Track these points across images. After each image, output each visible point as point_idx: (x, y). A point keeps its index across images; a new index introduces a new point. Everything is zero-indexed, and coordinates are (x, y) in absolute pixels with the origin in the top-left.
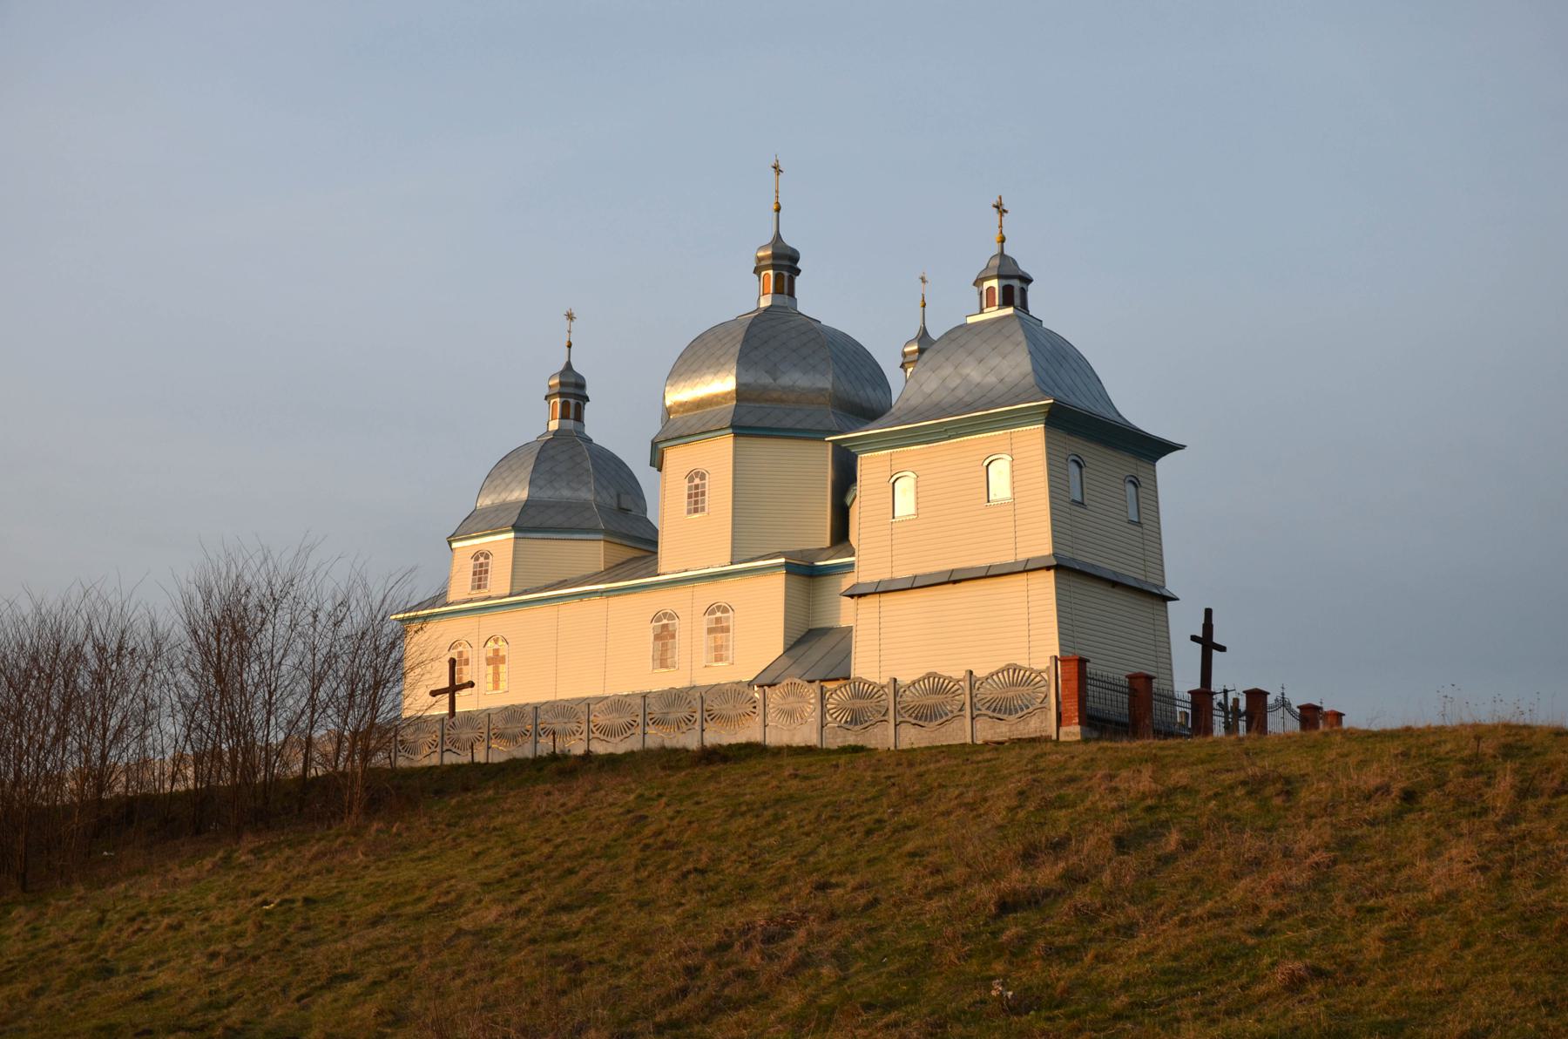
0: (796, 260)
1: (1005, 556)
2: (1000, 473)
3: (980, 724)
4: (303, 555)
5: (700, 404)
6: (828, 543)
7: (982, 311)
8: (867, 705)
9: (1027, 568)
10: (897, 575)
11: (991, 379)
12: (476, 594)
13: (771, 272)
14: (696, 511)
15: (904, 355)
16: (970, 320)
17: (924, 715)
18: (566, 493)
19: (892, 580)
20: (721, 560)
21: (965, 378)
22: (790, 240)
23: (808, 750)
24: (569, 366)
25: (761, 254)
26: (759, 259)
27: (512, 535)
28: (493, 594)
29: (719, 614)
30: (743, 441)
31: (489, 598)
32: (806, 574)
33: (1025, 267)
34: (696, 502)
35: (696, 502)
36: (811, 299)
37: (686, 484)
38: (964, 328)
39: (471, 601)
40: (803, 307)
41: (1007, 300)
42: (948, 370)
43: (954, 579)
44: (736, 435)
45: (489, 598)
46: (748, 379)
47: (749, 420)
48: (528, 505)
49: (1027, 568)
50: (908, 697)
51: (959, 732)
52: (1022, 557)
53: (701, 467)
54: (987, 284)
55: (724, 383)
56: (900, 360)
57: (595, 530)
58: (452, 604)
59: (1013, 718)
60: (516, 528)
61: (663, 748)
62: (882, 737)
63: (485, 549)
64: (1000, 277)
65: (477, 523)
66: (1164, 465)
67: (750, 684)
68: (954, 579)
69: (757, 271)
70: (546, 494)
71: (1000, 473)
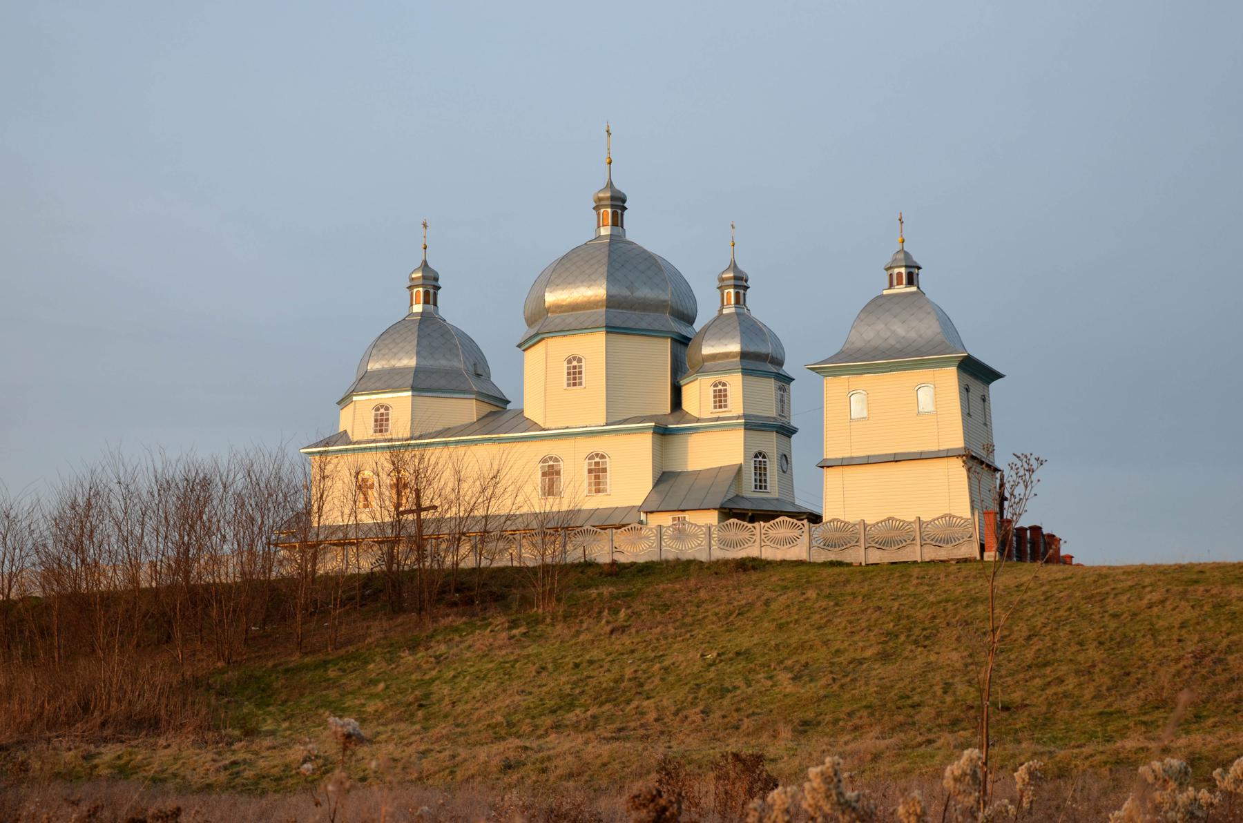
0: (624, 201)
1: (932, 447)
2: (925, 398)
3: (926, 549)
4: (772, 467)
5: (574, 307)
6: (669, 411)
7: (891, 286)
8: (848, 535)
9: (948, 455)
10: (854, 455)
11: (913, 335)
12: (379, 436)
13: (609, 210)
14: (574, 384)
15: (722, 280)
16: (885, 292)
17: (883, 544)
18: (444, 363)
19: (852, 458)
20: (598, 419)
21: (893, 332)
22: (618, 186)
23: (800, 563)
24: (425, 264)
25: (601, 195)
26: (600, 199)
27: (410, 393)
28: (394, 437)
29: (597, 460)
30: (611, 336)
31: (391, 440)
32: (663, 432)
33: (917, 259)
34: (575, 379)
35: (575, 379)
36: (636, 230)
37: (565, 365)
38: (882, 296)
39: (375, 441)
40: (629, 236)
41: (911, 282)
42: (880, 326)
43: (897, 459)
44: (607, 332)
45: (391, 440)
46: (615, 291)
47: (617, 323)
48: (418, 371)
49: (948, 455)
50: (873, 532)
51: (914, 553)
52: (944, 447)
53: (578, 353)
54: (896, 270)
55: (597, 291)
56: (717, 284)
57: (470, 392)
58: (388, 447)
59: (950, 545)
60: (413, 389)
61: (678, 560)
62: (856, 555)
63: (385, 403)
64: (906, 267)
65: (367, 382)
66: (995, 386)
67: (639, 509)
68: (897, 459)
69: (597, 208)
70: (429, 363)
71: (925, 398)
